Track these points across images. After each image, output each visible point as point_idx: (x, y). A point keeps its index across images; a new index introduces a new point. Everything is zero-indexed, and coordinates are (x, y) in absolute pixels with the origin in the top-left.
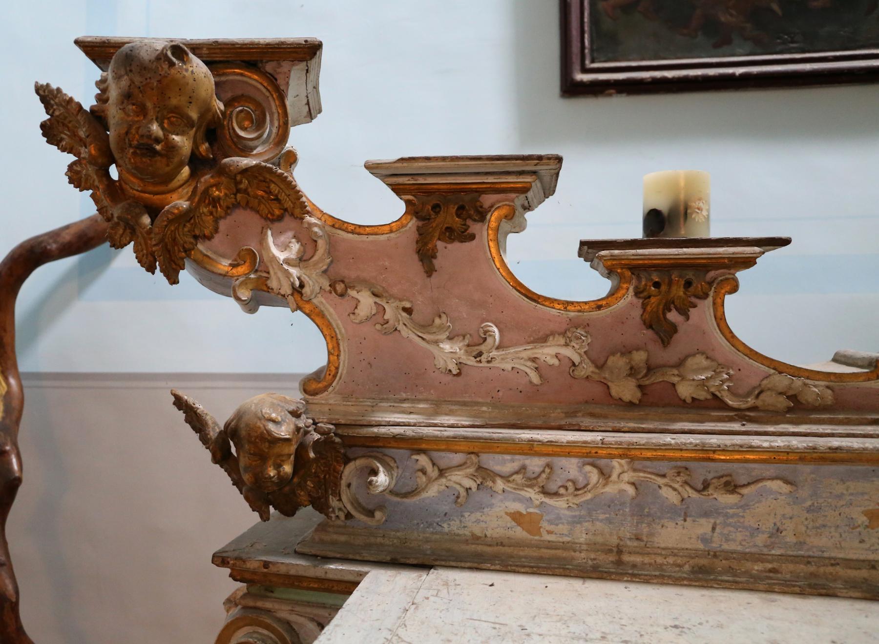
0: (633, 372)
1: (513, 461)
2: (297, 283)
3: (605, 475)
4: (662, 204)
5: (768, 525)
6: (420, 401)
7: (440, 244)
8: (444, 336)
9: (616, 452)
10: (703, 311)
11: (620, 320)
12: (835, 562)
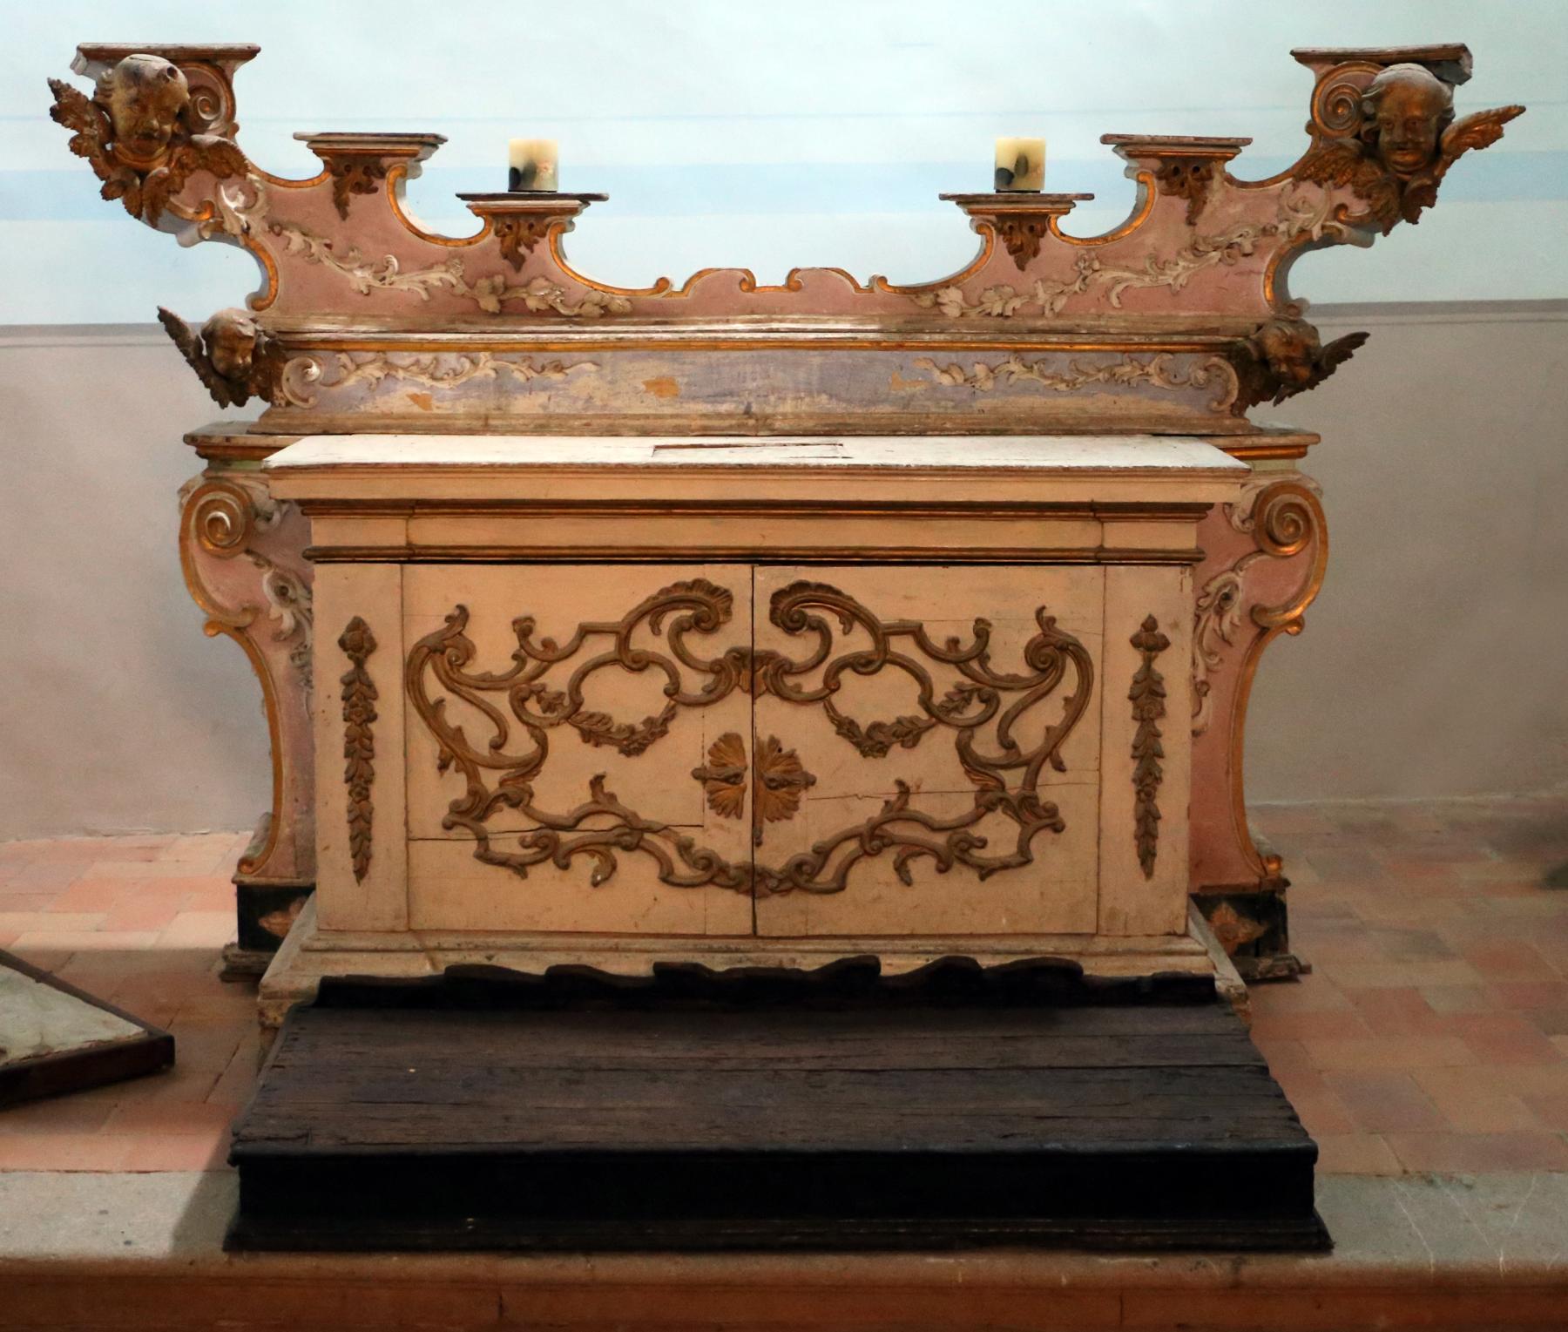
0: (494, 290)
1: (410, 356)
2: (245, 226)
3: (474, 363)
4: (520, 166)
5: (584, 395)
6: (339, 314)
7: (351, 195)
8: (356, 265)
9: (480, 346)
10: (543, 247)
11: (485, 252)
12: (625, 417)
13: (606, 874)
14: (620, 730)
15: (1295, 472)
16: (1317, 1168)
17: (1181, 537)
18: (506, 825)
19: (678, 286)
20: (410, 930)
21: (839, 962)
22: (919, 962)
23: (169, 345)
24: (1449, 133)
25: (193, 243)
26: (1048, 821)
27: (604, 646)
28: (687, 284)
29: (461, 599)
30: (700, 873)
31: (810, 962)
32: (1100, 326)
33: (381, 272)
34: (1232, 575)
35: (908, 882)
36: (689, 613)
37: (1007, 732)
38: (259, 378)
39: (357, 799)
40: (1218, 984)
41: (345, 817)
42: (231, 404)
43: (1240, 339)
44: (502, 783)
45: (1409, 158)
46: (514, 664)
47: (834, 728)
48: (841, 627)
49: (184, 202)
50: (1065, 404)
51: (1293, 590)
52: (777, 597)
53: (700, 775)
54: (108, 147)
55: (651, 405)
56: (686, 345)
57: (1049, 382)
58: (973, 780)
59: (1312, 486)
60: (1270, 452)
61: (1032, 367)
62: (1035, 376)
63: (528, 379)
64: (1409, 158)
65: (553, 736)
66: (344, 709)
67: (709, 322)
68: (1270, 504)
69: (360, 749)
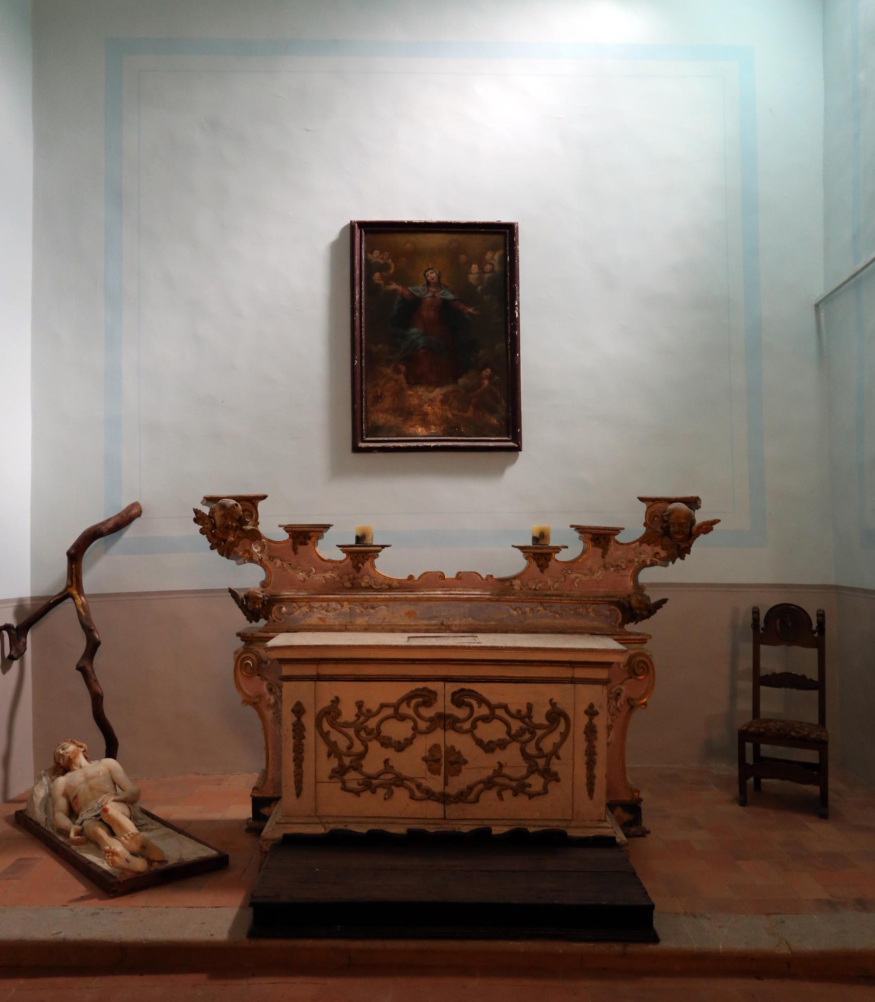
0: (349, 580)
3: (342, 606)
4: (359, 535)
7: (299, 546)
10: (368, 564)
12: (397, 625)
13: (389, 796)
14: (395, 742)
15: (642, 649)
16: (654, 911)
17: (603, 674)
18: (352, 777)
19: (416, 577)
20: (317, 816)
21: (478, 829)
22: (506, 829)
23: (228, 596)
24: (694, 528)
25: (241, 564)
26: (554, 778)
27: (390, 711)
28: (420, 577)
29: (337, 694)
30: (424, 795)
31: (465, 829)
32: (571, 594)
33: (308, 573)
34: (620, 686)
35: (502, 799)
36: (421, 700)
37: (539, 745)
38: (264, 612)
39: (297, 767)
40: (617, 839)
41: (292, 774)
42: (254, 622)
43: (622, 600)
44: (351, 762)
45: (680, 537)
46: (356, 718)
47: (474, 743)
48: (477, 705)
49: (239, 550)
50: (559, 622)
51: (643, 692)
52: (454, 694)
53: (425, 759)
54: (213, 531)
55: (406, 621)
56: (419, 600)
57: (552, 614)
58: (526, 762)
59: (648, 654)
60: (635, 641)
61: (546, 609)
62: (548, 611)
63: (361, 612)
64: (680, 537)
65: (370, 744)
66: (293, 734)
67: (427, 591)
68: (633, 661)
69: (299, 750)
